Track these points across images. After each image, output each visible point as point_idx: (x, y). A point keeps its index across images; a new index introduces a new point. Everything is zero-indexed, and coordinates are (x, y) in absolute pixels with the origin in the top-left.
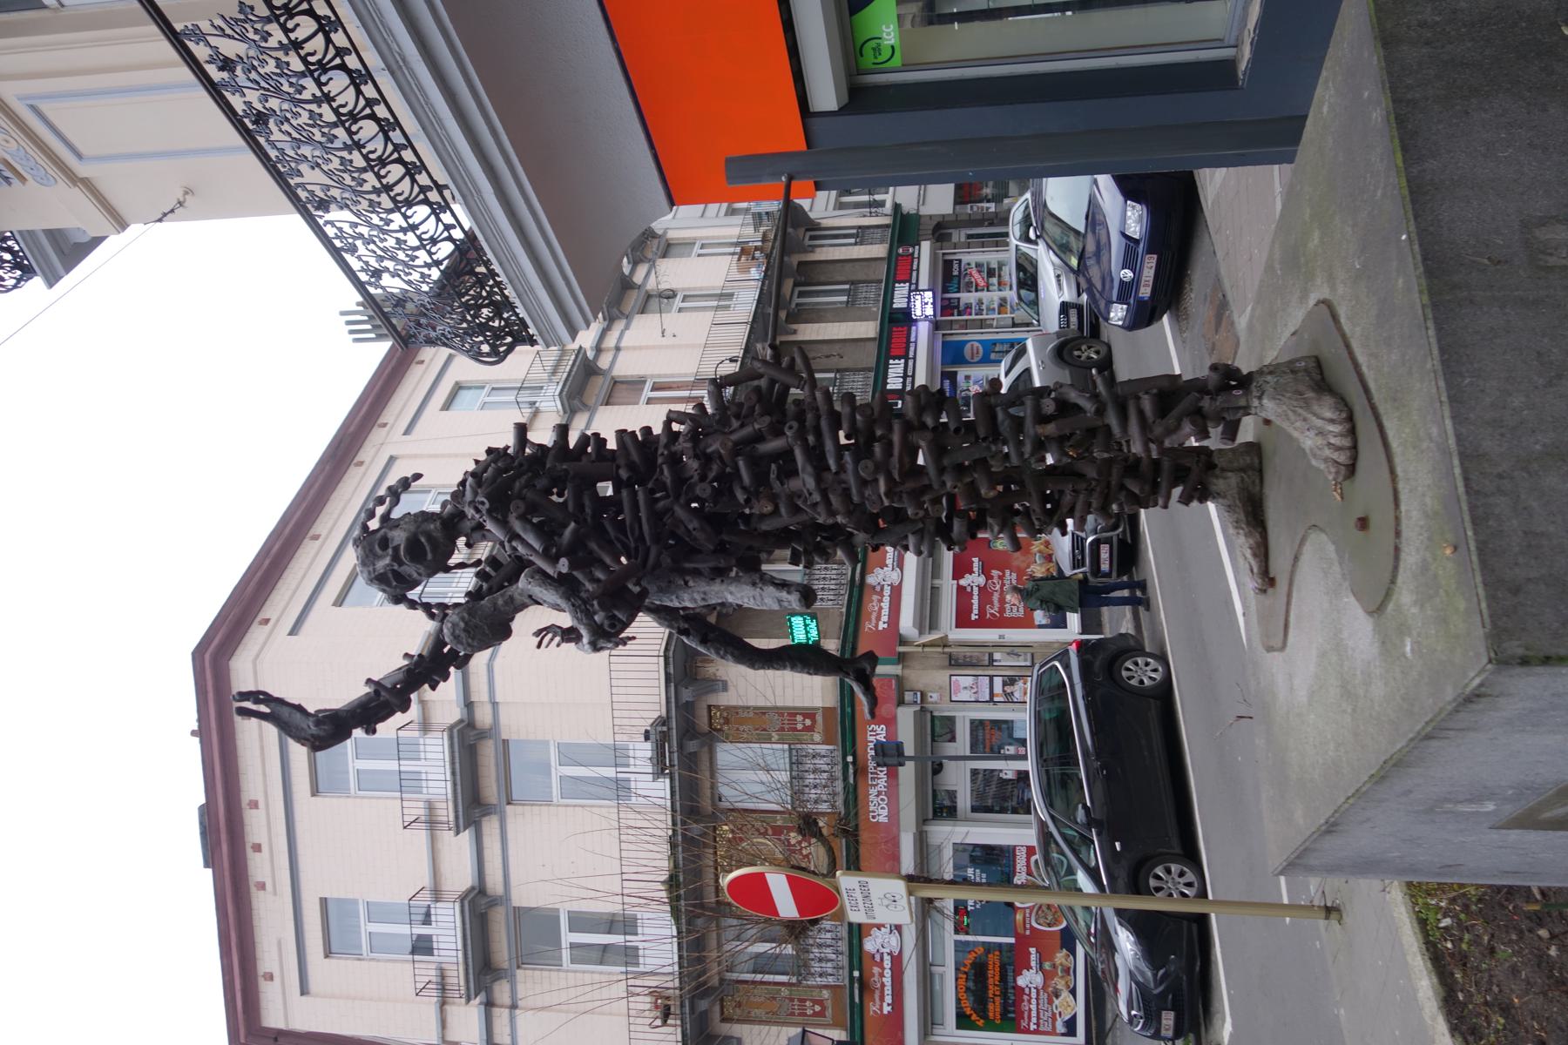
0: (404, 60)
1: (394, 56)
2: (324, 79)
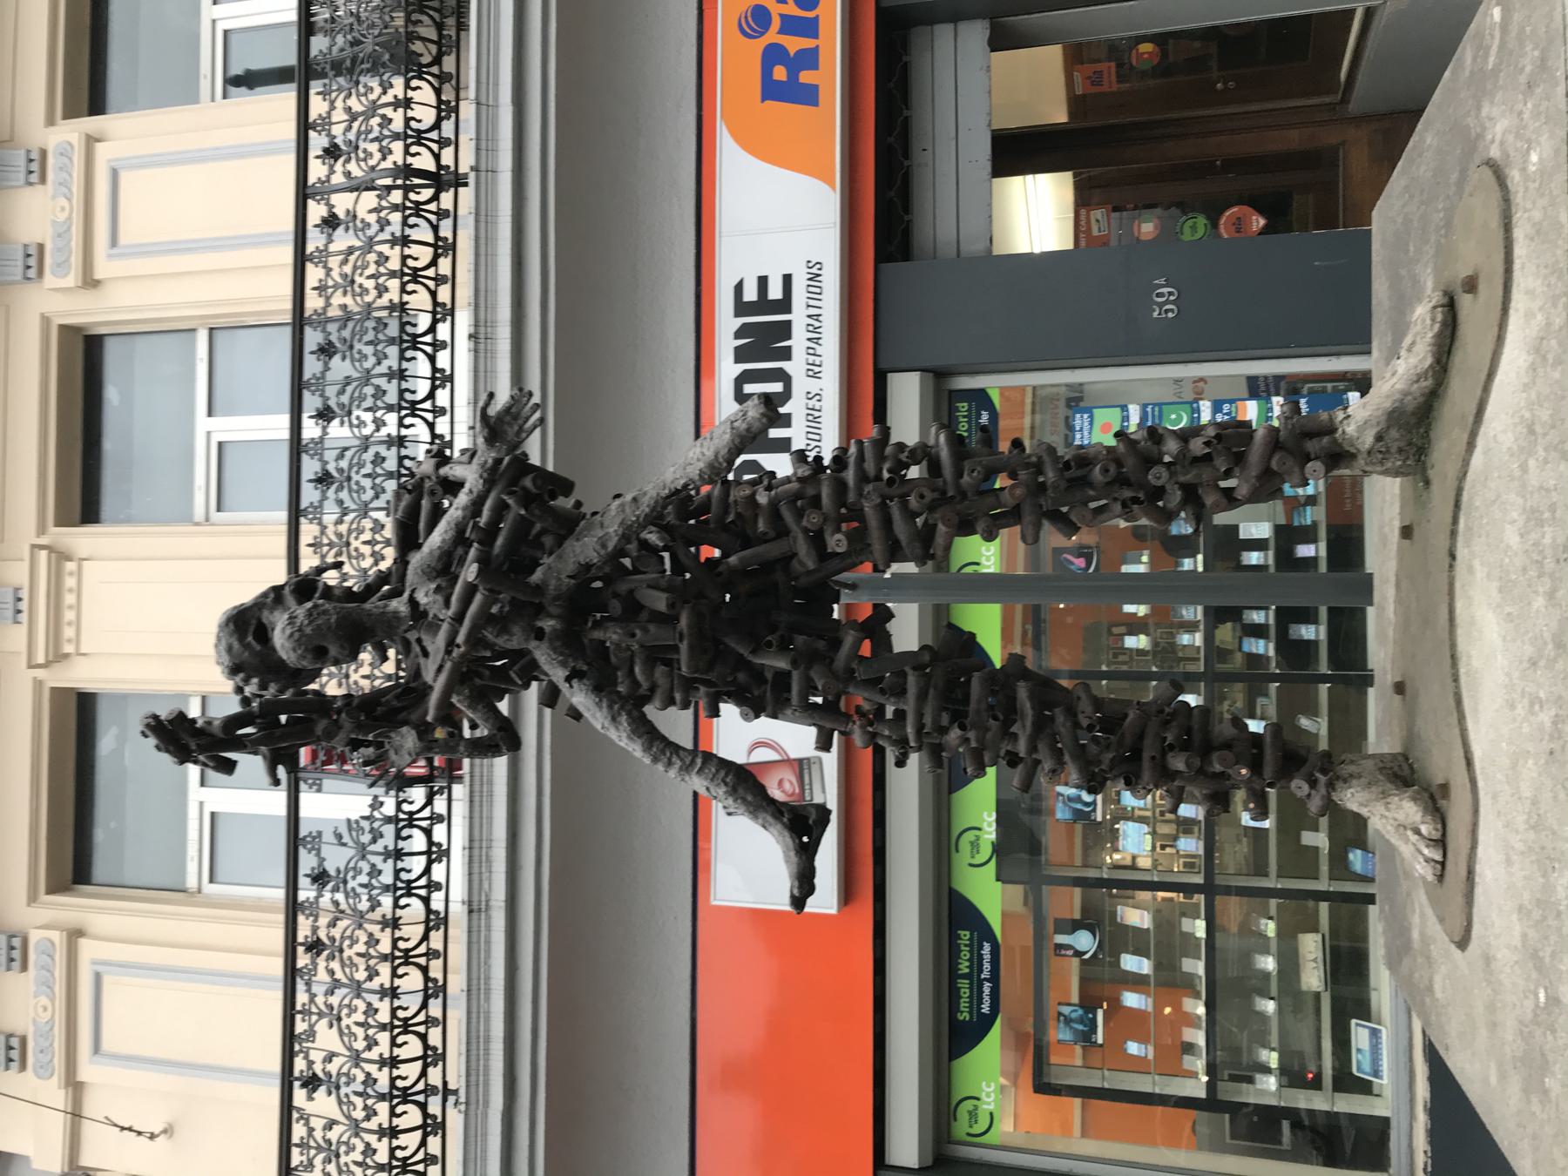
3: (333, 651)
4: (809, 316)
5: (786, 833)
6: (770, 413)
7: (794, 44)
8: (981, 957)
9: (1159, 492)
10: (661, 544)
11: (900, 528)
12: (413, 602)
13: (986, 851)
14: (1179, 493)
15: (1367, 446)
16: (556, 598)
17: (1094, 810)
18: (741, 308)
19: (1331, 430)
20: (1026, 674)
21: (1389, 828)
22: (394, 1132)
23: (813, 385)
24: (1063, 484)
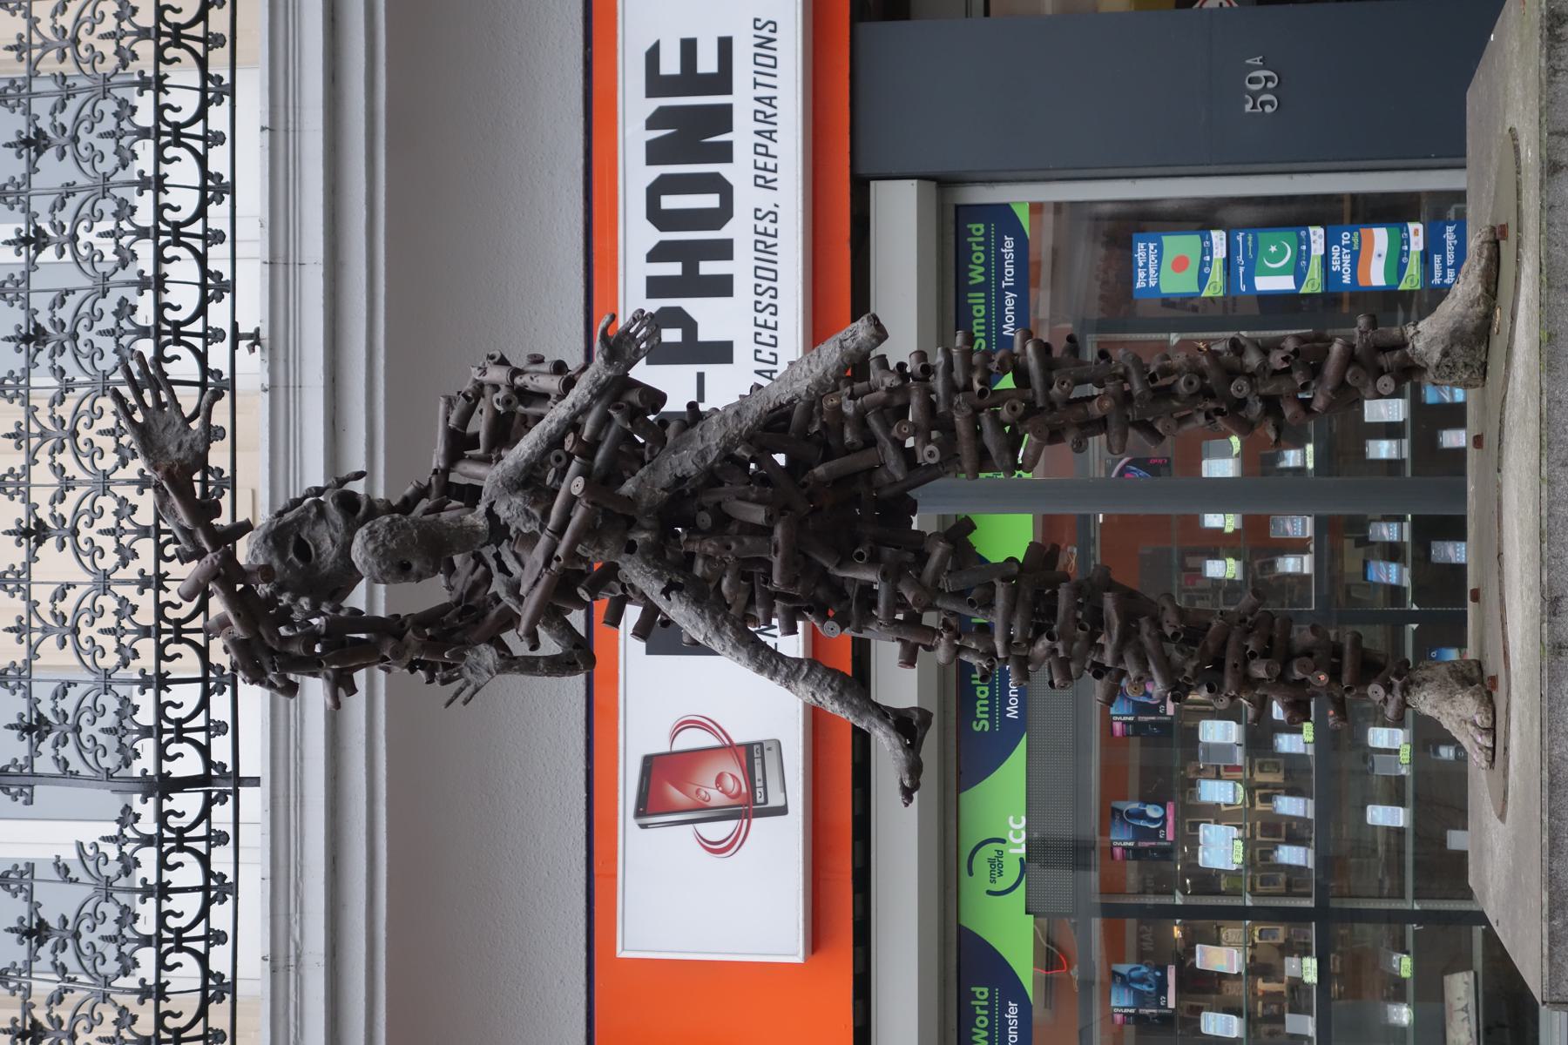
0: (298, 957)
1: (288, 941)
2: (170, 650)
3: (416, 566)
4: (758, 99)
5: (892, 734)
6: (879, 334)
9: (1242, 403)
10: (748, 456)
11: (990, 439)
12: (490, 513)
13: (1012, 871)
14: (1260, 405)
15: (1435, 361)
16: (648, 510)
17: (1164, 827)
18: (656, 84)
19: (1402, 344)
20: (1110, 586)
21: (1454, 724)
23: (765, 200)
24: (1148, 396)
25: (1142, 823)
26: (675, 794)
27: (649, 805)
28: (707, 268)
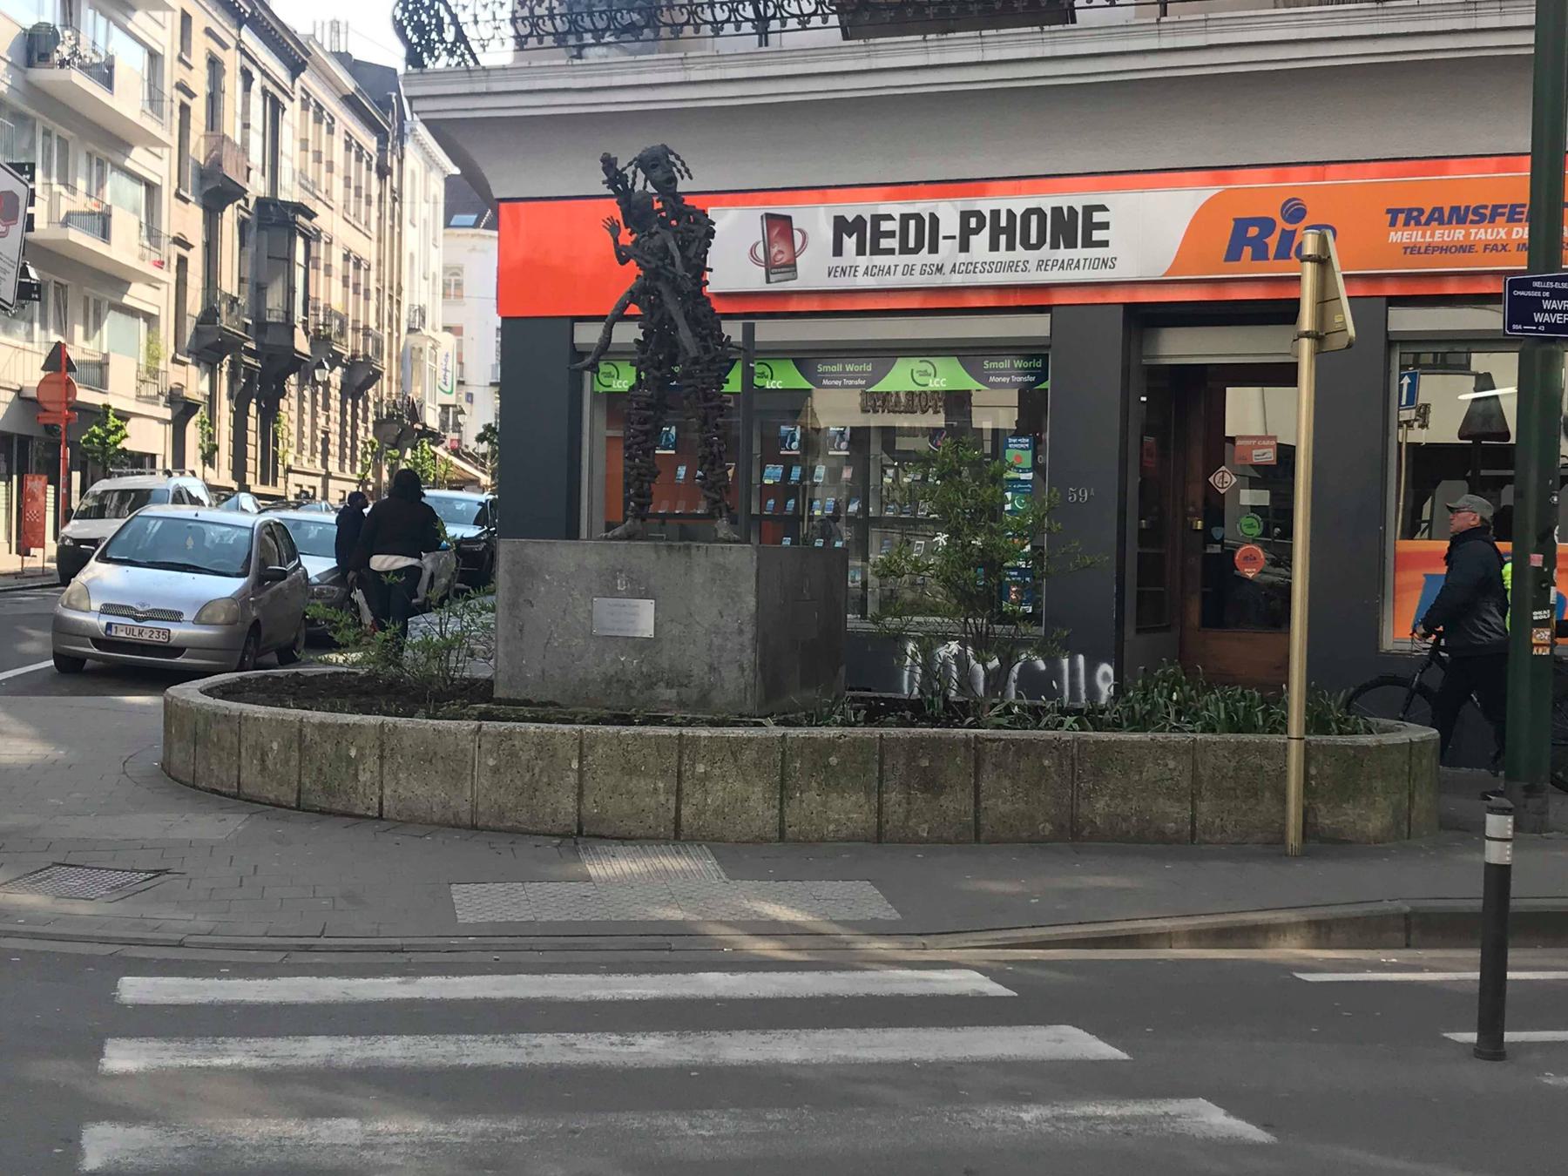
7: (1273, 242)
8: (856, 379)
18: (1089, 210)
22: (552, 17)
23: (1032, 266)
25: (837, 440)
26: (775, 232)
27: (770, 219)
28: (1003, 238)
